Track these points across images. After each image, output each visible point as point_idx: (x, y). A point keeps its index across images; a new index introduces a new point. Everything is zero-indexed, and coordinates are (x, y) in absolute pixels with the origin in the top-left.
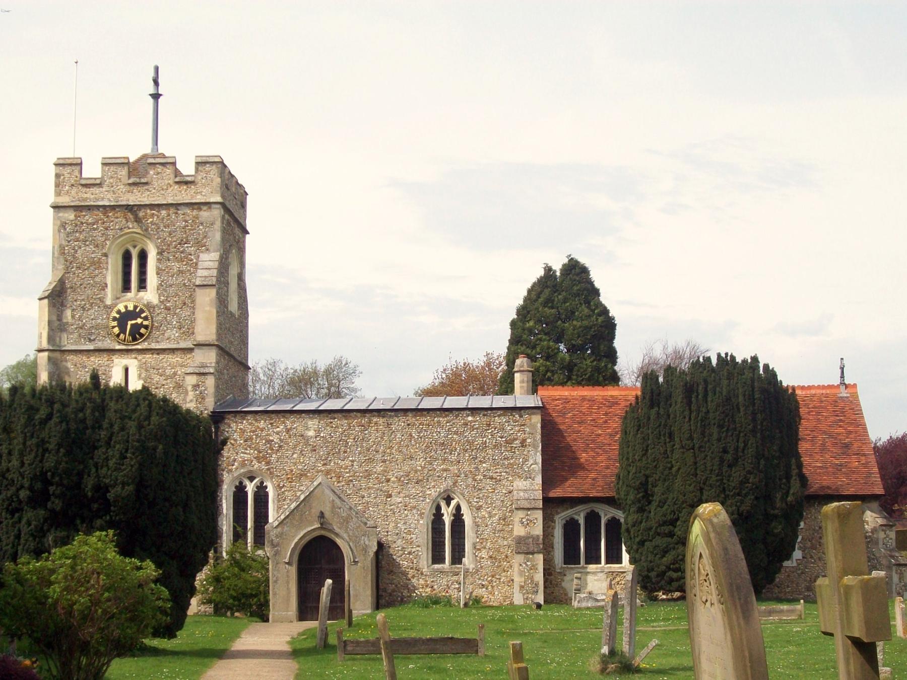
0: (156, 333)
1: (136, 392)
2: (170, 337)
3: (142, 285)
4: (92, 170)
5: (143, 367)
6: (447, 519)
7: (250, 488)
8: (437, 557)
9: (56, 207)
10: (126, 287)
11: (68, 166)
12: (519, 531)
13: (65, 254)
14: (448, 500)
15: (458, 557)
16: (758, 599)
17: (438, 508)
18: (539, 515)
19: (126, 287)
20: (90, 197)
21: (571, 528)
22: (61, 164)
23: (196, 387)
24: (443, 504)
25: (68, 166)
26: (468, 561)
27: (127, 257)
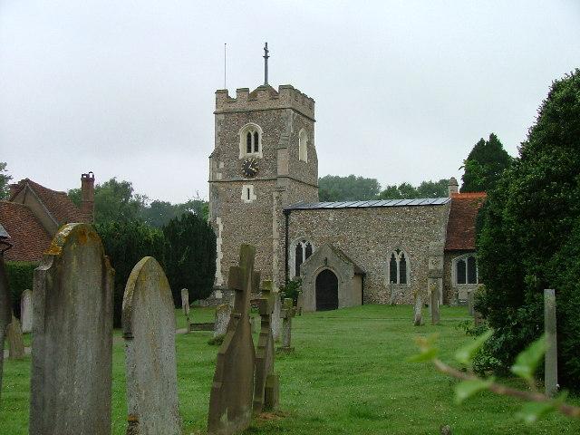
0: (261, 172)
1: (98, 187)
2: (267, 173)
3: (256, 150)
4: (233, 95)
5: (256, 189)
6: (398, 261)
7: (304, 246)
8: (393, 279)
9: (215, 113)
10: (249, 151)
11: (222, 94)
12: (431, 267)
13: (221, 137)
14: (398, 251)
15: (403, 280)
16: (208, 236)
17: (393, 255)
18: (441, 259)
19: (249, 151)
20: (232, 107)
21: (461, 265)
22: (218, 92)
23: (277, 198)
24: (395, 253)
25: (222, 94)
26: (409, 284)
27: (249, 136)
